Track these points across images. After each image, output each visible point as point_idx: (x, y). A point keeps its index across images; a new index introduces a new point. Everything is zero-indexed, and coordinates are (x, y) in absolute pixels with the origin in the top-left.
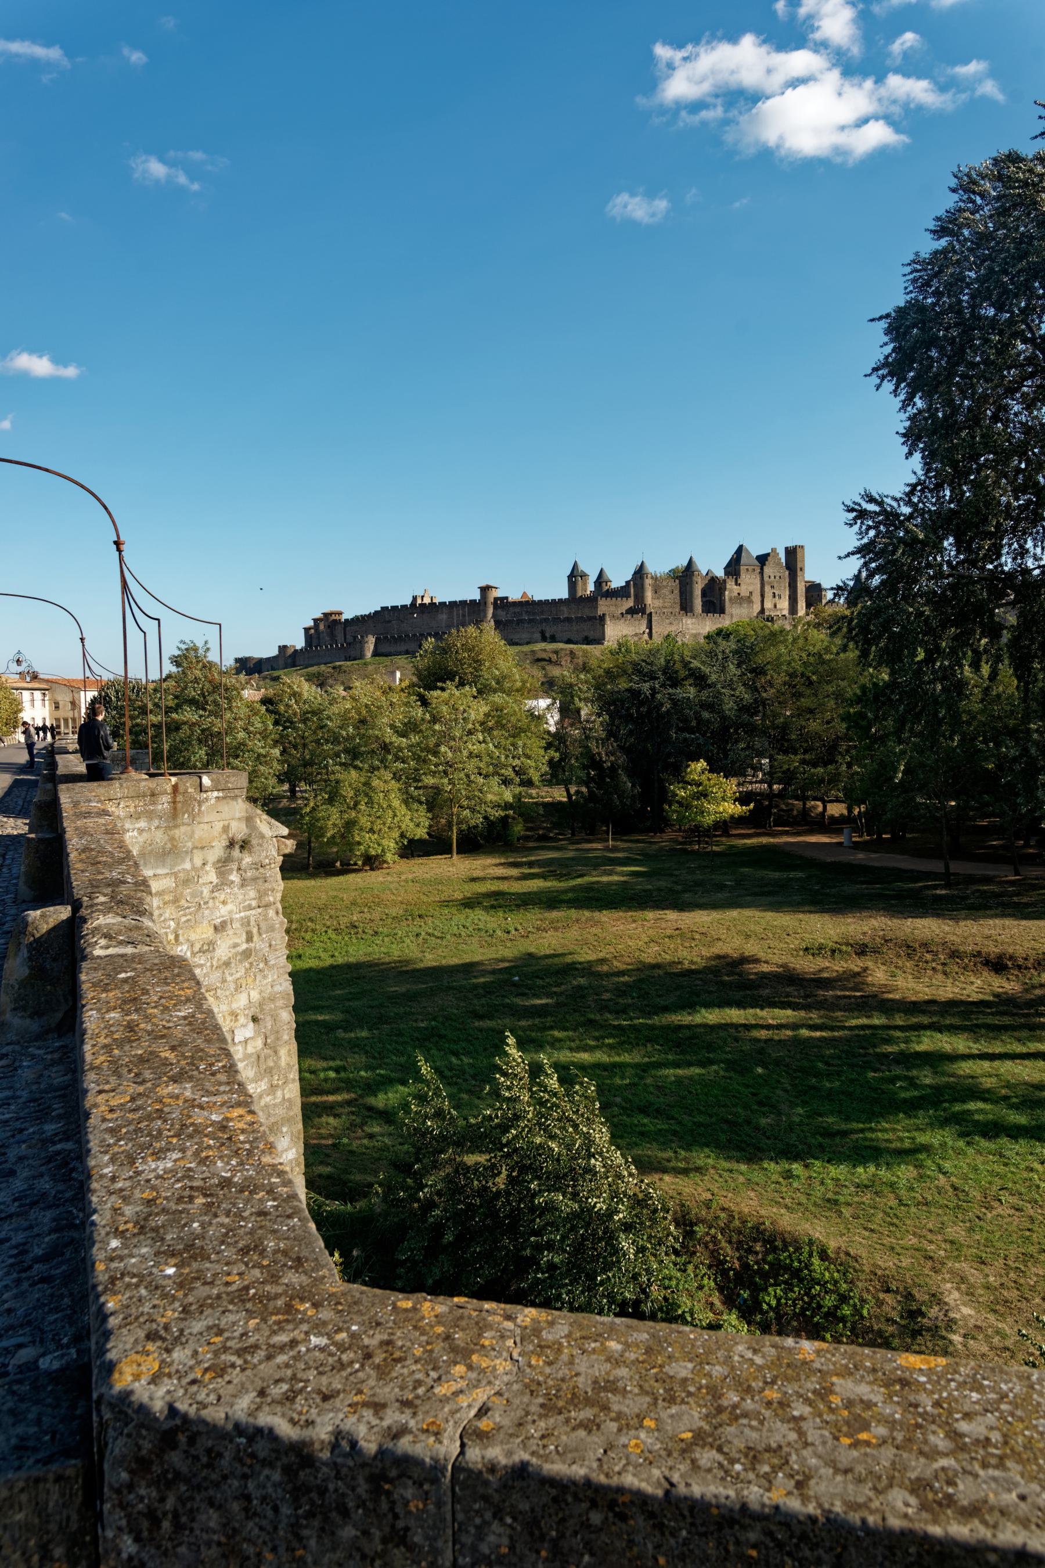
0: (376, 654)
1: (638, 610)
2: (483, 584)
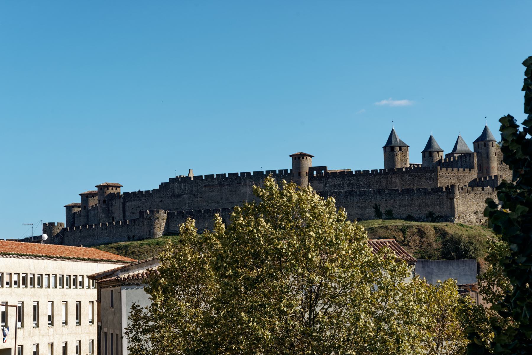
2: (296, 152)
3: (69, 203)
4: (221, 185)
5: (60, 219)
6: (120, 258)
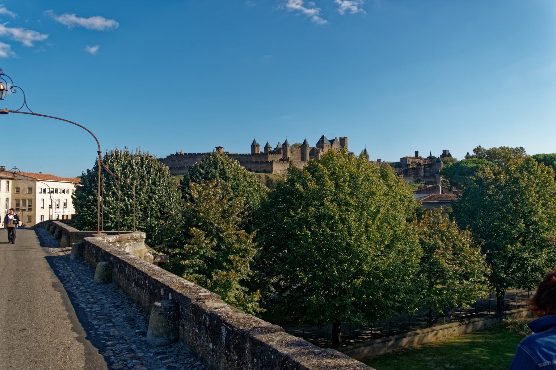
4: (190, 157)
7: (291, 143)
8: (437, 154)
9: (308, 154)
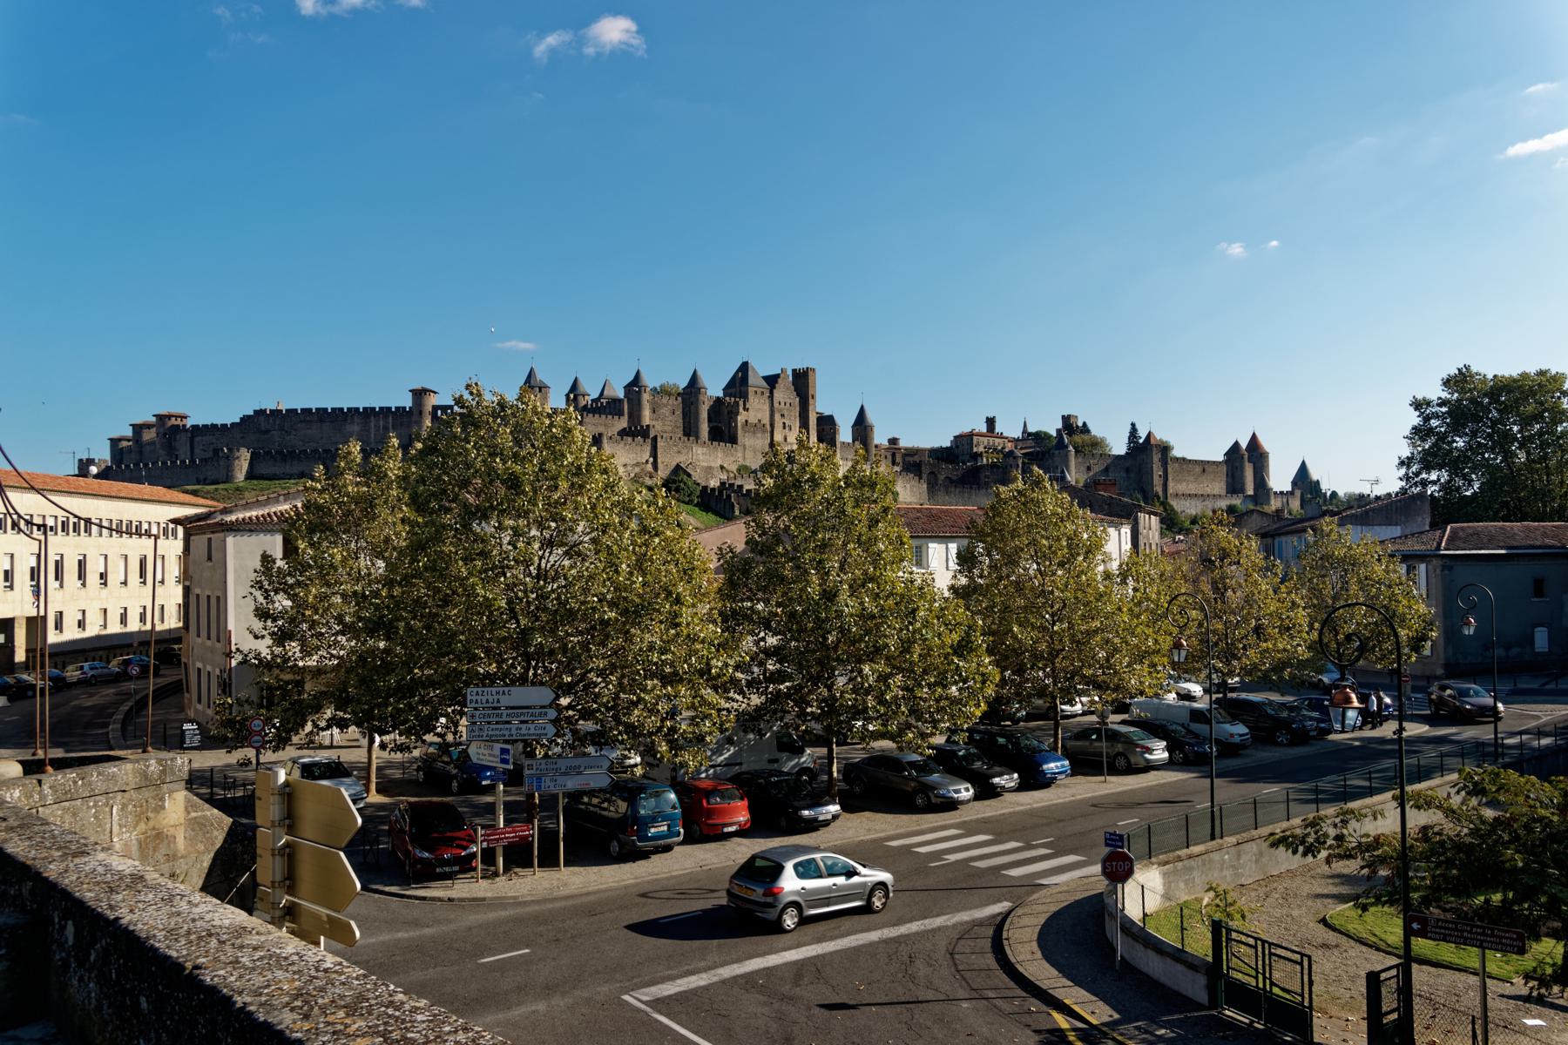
0: (250, 476)
1: (636, 431)
2: (418, 386)
3: (115, 435)
4: (321, 421)
5: (103, 454)
6: (201, 501)
7: (651, 381)
8: (1052, 427)
9: (704, 415)
